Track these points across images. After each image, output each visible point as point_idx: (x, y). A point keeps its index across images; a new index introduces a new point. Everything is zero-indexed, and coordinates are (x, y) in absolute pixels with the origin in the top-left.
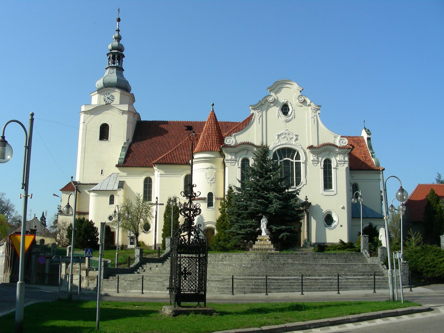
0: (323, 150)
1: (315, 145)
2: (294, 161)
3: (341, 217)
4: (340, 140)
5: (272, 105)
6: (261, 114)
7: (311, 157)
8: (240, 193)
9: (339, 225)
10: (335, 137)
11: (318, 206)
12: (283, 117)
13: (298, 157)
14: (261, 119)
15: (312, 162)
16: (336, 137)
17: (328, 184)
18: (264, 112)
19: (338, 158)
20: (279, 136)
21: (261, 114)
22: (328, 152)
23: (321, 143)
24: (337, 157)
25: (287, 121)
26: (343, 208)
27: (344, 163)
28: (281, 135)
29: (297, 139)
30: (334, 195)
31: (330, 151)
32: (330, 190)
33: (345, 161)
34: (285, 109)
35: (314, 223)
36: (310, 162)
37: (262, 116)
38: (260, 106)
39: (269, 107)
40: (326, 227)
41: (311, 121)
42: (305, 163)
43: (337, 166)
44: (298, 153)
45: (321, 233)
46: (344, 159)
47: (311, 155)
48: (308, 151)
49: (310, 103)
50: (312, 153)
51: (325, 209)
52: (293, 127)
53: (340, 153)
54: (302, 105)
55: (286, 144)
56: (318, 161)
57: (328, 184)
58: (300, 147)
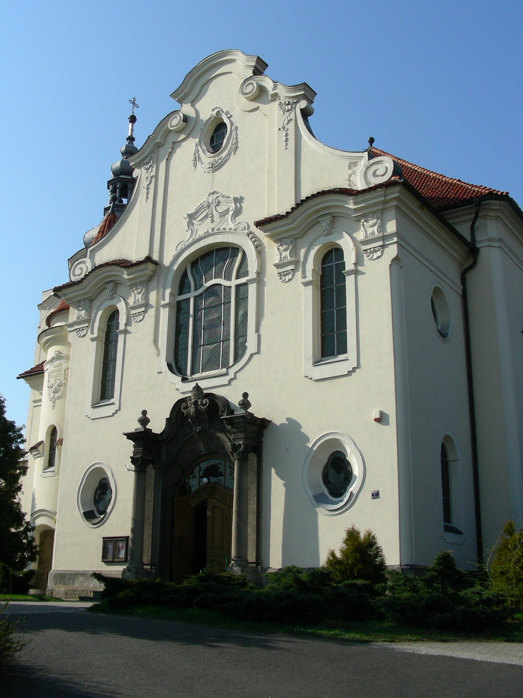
0: (310, 217)
3: (378, 461)
4: (368, 168)
5: (182, 136)
6: (153, 173)
7: (274, 253)
8: (356, 574)
9: (366, 494)
10: (352, 165)
11: (293, 425)
12: (207, 158)
13: (242, 272)
14: (152, 186)
15: (275, 271)
16: (355, 164)
17: (331, 339)
18: (163, 165)
19: (360, 236)
20: (191, 217)
21: (153, 173)
22: (325, 223)
23: (305, 193)
24: (357, 230)
26: (381, 419)
27: (383, 247)
28: (196, 213)
29: (237, 212)
30: (350, 373)
31: (334, 218)
32: (341, 357)
33: (384, 238)
35: (277, 490)
36: (271, 272)
37: (156, 176)
38: (152, 152)
39: (175, 145)
40: (320, 499)
41: (276, 138)
42: (260, 279)
43: (359, 262)
44: (244, 254)
45: (301, 530)
46: (382, 228)
47: (275, 246)
48: (259, 233)
49: (275, 88)
50: (279, 240)
51: (314, 432)
53: (364, 215)
54: (255, 105)
55: (207, 235)
56: (296, 263)
57: (331, 339)
58: (246, 231)
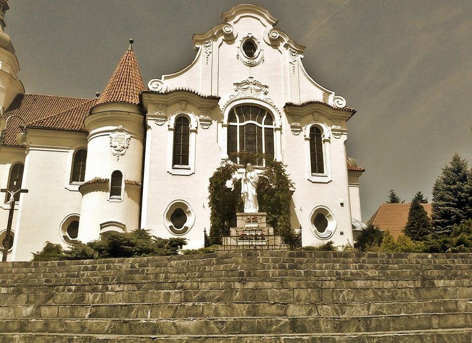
1: (296, 102)
2: (263, 126)
4: (335, 99)
13: (270, 119)
25: (251, 65)
34: (250, 46)
52: (258, 73)
